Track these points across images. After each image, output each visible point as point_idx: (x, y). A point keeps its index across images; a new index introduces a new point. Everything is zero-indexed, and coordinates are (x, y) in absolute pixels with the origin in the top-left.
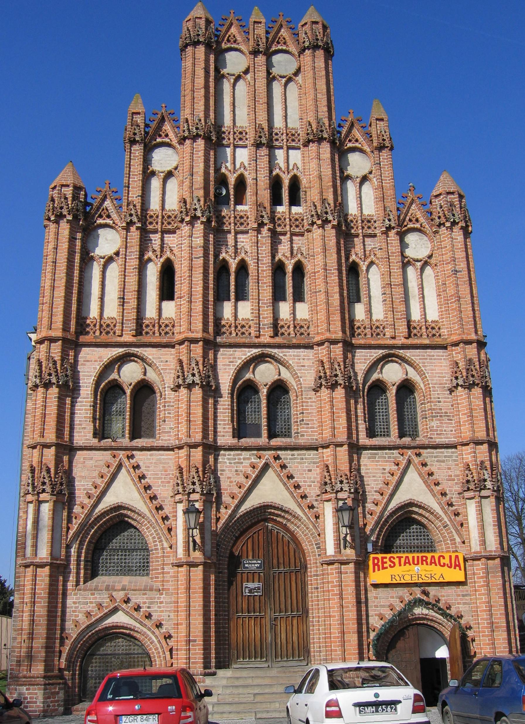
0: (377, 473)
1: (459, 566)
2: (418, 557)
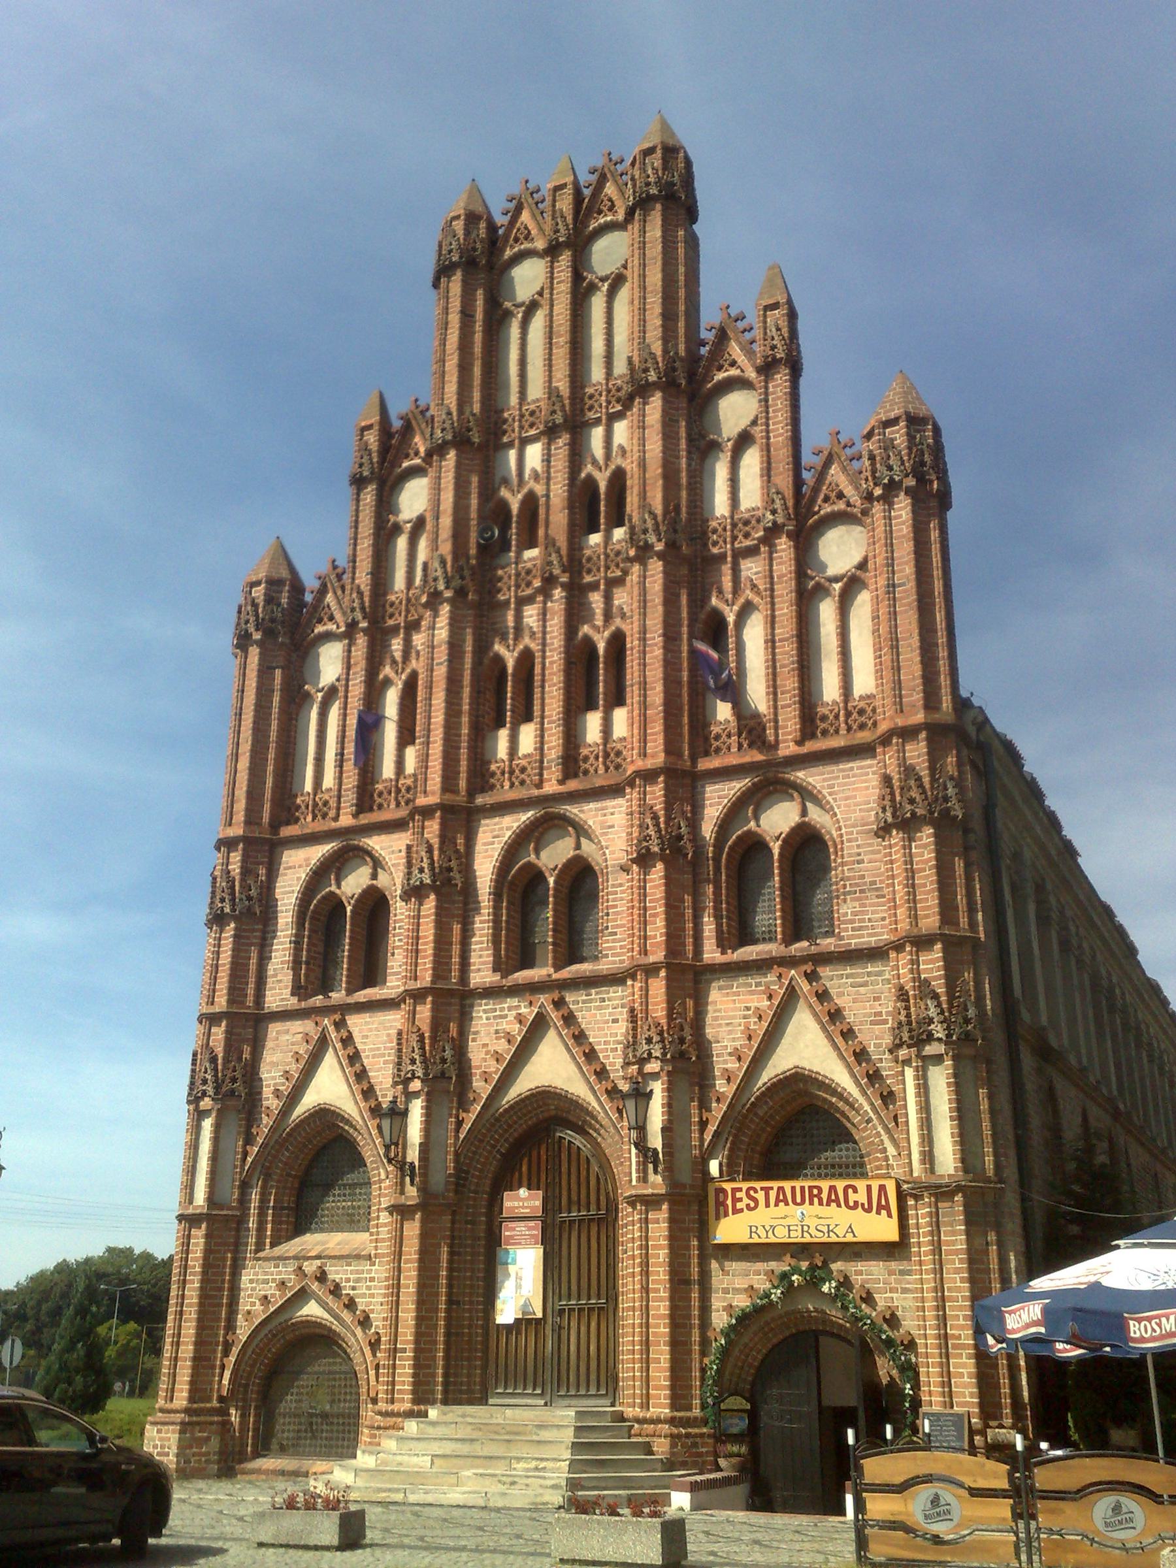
0: (734, 1017)
1: (887, 1208)
2: (802, 1188)
